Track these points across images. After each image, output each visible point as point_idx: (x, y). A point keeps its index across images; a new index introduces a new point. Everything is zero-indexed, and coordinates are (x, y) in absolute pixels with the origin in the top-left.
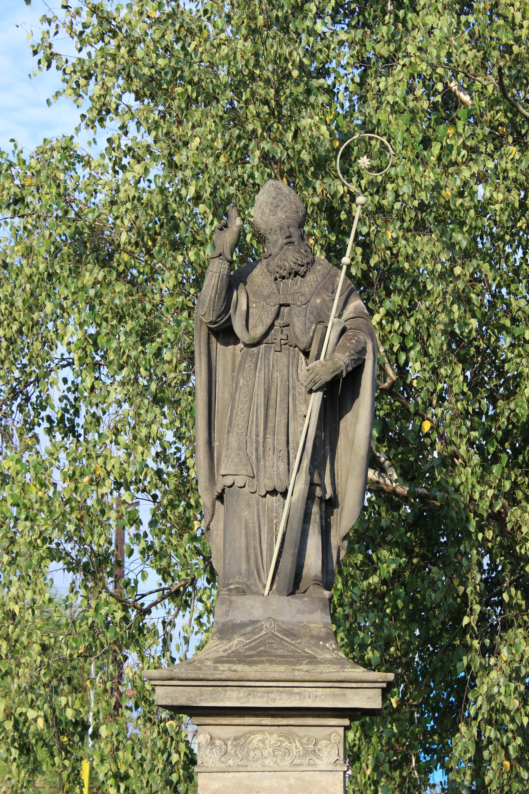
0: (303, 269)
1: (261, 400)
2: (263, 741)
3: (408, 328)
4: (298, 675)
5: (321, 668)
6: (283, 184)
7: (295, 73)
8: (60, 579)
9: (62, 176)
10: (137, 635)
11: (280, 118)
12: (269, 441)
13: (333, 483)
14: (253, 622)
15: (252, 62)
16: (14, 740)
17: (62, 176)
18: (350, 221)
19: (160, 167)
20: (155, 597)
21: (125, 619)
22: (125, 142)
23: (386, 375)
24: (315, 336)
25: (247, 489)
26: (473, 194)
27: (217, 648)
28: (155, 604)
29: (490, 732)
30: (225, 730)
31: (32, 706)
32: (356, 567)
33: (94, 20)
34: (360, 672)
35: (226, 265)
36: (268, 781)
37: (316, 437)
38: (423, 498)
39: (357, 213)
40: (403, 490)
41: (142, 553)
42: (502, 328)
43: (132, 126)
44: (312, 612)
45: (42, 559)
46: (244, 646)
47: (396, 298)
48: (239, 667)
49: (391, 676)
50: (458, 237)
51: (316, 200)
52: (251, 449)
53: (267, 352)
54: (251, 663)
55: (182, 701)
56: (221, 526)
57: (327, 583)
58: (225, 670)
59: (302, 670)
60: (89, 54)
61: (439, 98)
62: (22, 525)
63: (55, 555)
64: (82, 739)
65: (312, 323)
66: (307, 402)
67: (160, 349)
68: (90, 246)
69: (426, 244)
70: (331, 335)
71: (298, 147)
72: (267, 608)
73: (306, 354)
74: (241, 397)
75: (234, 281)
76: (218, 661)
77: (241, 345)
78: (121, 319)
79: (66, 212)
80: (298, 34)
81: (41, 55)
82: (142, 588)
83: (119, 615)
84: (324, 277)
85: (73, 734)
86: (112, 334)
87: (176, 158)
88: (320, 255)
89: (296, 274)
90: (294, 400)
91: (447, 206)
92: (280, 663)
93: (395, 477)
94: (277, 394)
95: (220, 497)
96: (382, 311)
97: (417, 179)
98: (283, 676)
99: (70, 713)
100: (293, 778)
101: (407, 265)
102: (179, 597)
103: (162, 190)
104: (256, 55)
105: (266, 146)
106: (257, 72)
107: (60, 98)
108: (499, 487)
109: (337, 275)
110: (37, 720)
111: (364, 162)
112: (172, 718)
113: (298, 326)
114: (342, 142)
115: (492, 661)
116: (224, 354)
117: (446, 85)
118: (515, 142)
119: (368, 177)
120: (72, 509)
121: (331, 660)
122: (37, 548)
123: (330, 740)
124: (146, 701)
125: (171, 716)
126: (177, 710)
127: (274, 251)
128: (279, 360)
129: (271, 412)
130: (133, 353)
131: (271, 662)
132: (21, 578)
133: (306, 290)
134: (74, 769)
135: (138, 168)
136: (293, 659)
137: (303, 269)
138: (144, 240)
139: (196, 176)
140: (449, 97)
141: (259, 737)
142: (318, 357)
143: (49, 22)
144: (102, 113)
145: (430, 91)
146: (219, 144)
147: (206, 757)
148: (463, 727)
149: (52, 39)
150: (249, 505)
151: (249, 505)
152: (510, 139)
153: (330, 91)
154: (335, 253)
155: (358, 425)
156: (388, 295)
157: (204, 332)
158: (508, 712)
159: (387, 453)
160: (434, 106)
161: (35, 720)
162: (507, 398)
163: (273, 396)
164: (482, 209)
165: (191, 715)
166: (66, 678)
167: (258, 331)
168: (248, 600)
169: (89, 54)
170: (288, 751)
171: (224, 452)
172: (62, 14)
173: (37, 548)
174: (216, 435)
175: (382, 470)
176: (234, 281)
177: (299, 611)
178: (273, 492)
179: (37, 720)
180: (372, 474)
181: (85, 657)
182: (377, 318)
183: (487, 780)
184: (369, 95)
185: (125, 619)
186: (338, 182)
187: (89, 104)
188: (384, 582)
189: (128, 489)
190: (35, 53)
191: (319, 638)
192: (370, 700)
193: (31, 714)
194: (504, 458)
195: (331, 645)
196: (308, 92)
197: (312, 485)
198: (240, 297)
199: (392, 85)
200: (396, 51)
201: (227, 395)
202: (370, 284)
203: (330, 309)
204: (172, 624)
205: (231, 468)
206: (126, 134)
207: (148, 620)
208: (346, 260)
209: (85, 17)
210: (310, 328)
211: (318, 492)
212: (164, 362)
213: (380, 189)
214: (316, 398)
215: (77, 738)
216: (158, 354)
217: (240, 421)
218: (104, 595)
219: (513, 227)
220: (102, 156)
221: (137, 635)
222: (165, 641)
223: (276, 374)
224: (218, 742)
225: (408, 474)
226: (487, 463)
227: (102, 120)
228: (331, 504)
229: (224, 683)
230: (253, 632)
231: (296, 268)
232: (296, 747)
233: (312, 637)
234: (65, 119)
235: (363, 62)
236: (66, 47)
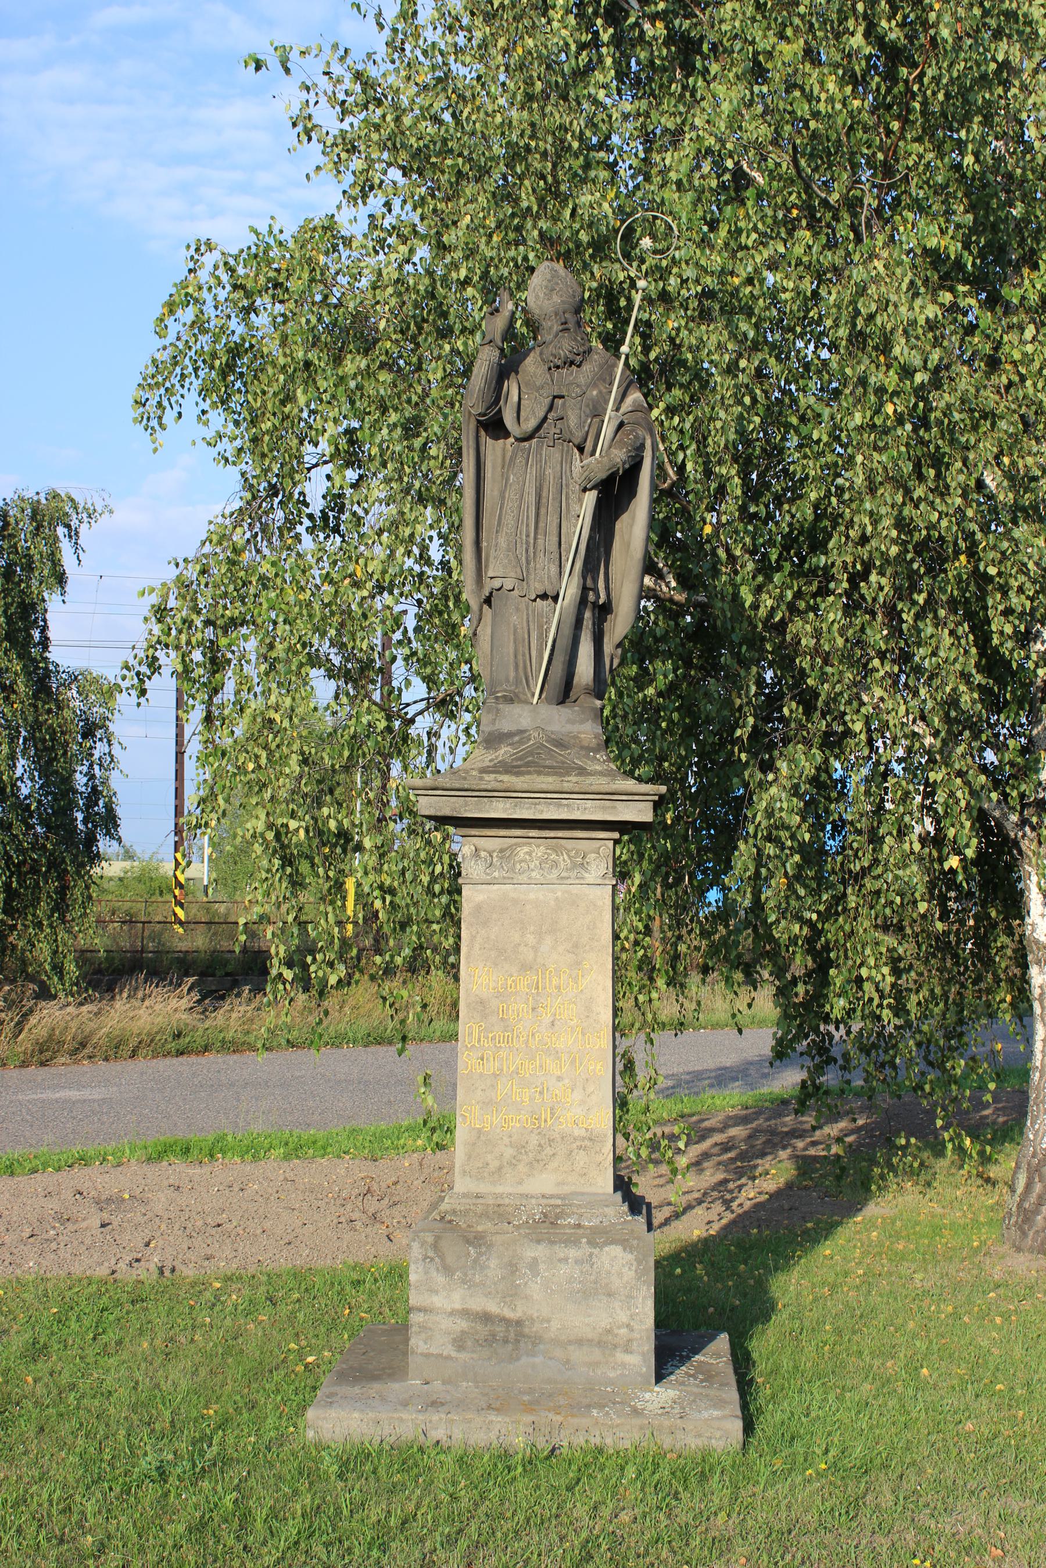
0: (578, 359)
1: (533, 499)
2: (530, 854)
3: (687, 425)
4: (567, 786)
5: (590, 780)
6: (559, 266)
7: (576, 145)
8: (323, 688)
9: (322, 259)
10: (400, 742)
11: (557, 195)
12: (540, 541)
13: (607, 588)
14: (521, 732)
15: (528, 132)
16: (275, 852)
17: (322, 259)
18: (630, 307)
19: (426, 248)
20: (422, 705)
21: (389, 729)
22: (388, 221)
23: (665, 476)
25: (516, 592)
26: (762, 281)
27: (485, 757)
28: (421, 713)
29: (770, 849)
30: (491, 842)
31: (293, 815)
32: (629, 679)
33: (358, 88)
34: (630, 785)
35: (497, 353)
36: (534, 894)
37: (591, 538)
38: (702, 607)
39: (637, 298)
40: (680, 597)
41: (406, 659)
42: (788, 426)
43: (397, 203)
44: (582, 722)
45: (301, 665)
47: (677, 392)
48: (505, 778)
49: (663, 789)
50: (744, 326)
51: (595, 285)
52: (521, 550)
53: (539, 447)
54: (518, 774)
55: (447, 812)
56: (489, 631)
57: (598, 690)
58: (490, 780)
59: (571, 781)
60: (352, 125)
61: (727, 177)
62: (282, 629)
63: (314, 661)
64: (345, 851)
66: (580, 501)
67: (425, 444)
68: (353, 334)
69: (713, 335)
70: (607, 430)
71: (576, 226)
72: (535, 717)
73: (581, 450)
74: (511, 495)
75: (507, 368)
76: (484, 771)
77: (512, 440)
78: (384, 410)
79: (326, 297)
80: (579, 104)
81: (300, 128)
82: (406, 698)
83: (382, 725)
84: (601, 367)
85: (335, 845)
86: (375, 427)
87: (445, 239)
88: (596, 344)
89: (572, 363)
91: (735, 293)
92: (548, 774)
93: (673, 584)
94: (550, 492)
95: (488, 601)
96: (662, 405)
97: (703, 262)
98: (551, 788)
99: (332, 824)
100: (560, 891)
101: (689, 356)
102: (445, 706)
103: (430, 273)
104: (533, 125)
105: (543, 224)
106: (533, 144)
107: (322, 173)
108: (782, 596)
109: (615, 365)
110: (298, 829)
111: (646, 242)
112: (436, 829)
113: (573, 420)
114: (623, 222)
115: (771, 777)
116: (494, 449)
117: (736, 164)
118: (809, 227)
119: (651, 261)
120: (332, 613)
121: (601, 771)
122: (296, 653)
123: (599, 854)
124: (411, 812)
126: (442, 821)
127: (549, 338)
128: (552, 456)
129: (543, 511)
130: (398, 448)
131: (539, 773)
132: (280, 685)
133: (582, 380)
134: (337, 881)
135: (403, 249)
136: (562, 770)
137: (578, 359)
138: (410, 330)
139: (467, 258)
140: (739, 174)
141: (526, 849)
142: (593, 453)
143: (308, 89)
144: (366, 188)
145: (719, 167)
146: (491, 222)
147: (471, 869)
148: (742, 845)
149: (311, 110)
150: (518, 609)
151: (518, 609)
152: (804, 223)
153: (612, 166)
154: (612, 342)
155: (634, 527)
156: (669, 389)
157: (473, 424)
158: (788, 828)
159: (666, 559)
160: (723, 186)
161: (297, 830)
162: (791, 501)
163: (544, 494)
164: (773, 294)
165: (456, 826)
166: (326, 787)
167: (530, 425)
168: (516, 709)
169: (352, 125)
170: (556, 864)
171: (492, 553)
172: (323, 82)
173: (296, 653)
174: (484, 535)
175: (660, 576)
176: (507, 368)
177: (569, 721)
178: (544, 596)
179: (298, 829)
180: (648, 581)
181: (347, 769)
182: (655, 413)
183: (763, 897)
184: (654, 171)
185: (389, 729)
186: (617, 266)
187: (351, 179)
188: (660, 694)
189: (391, 593)
190: (294, 125)
191: (589, 749)
192: (642, 813)
193: (293, 824)
194: (787, 567)
195: (601, 756)
196: (587, 166)
197: (585, 590)
198: (512, 387)
199: (676, 161)
200: (683, 123)
201: (496, 493)
202: (651, 377)
203: (607, 402)
204: (437, 734)
205: (500, 570)
206: (390, 211)
207: (412, 731)
208: (624, 349)
209: (348, 83)
211: (591, 597)
212: (431, 458)
213: (662, 273)
214: (590, 498)
215: (339, 850)
216: (424, 448)
217: (509, 520)
218: (366, 703)
219: (805, 317)
220: (365, 236)
221: (400, 742)
222: (429, 752)
223: (549, 471)
224: (483, 854)
225: (685, 581)
226: (766, 569)
227: (365, 196)
228: (604, 610)
229: (490, 794)
230: (521, 742)
231: (571, 356)
232: (564, 860)
233: (582, 748)
234: (325, 197)
235: (648, 139)
236: (327, 118)
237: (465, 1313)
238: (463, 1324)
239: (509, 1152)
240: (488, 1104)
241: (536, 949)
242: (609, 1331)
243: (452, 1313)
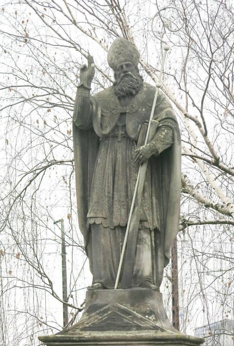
24: (141, 131)
46: (99, 320)
65: (139, 123)
70: (150, 130)
90: (130, 170)
125: (145, 243)
129: (116, 178)
210: (138, 126)
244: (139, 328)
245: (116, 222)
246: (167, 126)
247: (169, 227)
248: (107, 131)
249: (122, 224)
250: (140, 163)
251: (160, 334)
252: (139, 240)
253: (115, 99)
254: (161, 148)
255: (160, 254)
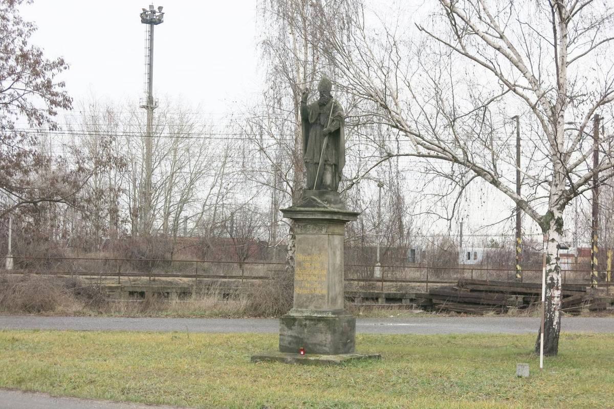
36: (311, 236)
100: (316, 236)
109: (160, 280)
237: (291, 336)
238: (290, 339)
239: (305, 299)
240: (300, 288)
241: (311, 250)
242: (321, 342)
243: (288, 336)
244: (318, 207)
245: (315, 161)
246: (337, 120)
247: (340, 164)
248: (313, 121)
249: (317, 162)
250: (325, 136)
251: (326, 210)
252: (325, 169)
253: (318, 107)
254: (333, 129)
255: (337, 175)
